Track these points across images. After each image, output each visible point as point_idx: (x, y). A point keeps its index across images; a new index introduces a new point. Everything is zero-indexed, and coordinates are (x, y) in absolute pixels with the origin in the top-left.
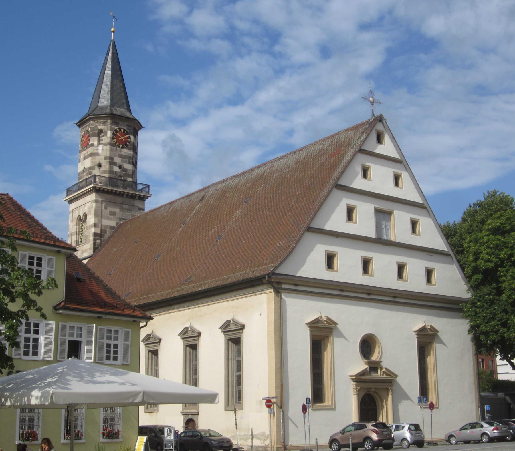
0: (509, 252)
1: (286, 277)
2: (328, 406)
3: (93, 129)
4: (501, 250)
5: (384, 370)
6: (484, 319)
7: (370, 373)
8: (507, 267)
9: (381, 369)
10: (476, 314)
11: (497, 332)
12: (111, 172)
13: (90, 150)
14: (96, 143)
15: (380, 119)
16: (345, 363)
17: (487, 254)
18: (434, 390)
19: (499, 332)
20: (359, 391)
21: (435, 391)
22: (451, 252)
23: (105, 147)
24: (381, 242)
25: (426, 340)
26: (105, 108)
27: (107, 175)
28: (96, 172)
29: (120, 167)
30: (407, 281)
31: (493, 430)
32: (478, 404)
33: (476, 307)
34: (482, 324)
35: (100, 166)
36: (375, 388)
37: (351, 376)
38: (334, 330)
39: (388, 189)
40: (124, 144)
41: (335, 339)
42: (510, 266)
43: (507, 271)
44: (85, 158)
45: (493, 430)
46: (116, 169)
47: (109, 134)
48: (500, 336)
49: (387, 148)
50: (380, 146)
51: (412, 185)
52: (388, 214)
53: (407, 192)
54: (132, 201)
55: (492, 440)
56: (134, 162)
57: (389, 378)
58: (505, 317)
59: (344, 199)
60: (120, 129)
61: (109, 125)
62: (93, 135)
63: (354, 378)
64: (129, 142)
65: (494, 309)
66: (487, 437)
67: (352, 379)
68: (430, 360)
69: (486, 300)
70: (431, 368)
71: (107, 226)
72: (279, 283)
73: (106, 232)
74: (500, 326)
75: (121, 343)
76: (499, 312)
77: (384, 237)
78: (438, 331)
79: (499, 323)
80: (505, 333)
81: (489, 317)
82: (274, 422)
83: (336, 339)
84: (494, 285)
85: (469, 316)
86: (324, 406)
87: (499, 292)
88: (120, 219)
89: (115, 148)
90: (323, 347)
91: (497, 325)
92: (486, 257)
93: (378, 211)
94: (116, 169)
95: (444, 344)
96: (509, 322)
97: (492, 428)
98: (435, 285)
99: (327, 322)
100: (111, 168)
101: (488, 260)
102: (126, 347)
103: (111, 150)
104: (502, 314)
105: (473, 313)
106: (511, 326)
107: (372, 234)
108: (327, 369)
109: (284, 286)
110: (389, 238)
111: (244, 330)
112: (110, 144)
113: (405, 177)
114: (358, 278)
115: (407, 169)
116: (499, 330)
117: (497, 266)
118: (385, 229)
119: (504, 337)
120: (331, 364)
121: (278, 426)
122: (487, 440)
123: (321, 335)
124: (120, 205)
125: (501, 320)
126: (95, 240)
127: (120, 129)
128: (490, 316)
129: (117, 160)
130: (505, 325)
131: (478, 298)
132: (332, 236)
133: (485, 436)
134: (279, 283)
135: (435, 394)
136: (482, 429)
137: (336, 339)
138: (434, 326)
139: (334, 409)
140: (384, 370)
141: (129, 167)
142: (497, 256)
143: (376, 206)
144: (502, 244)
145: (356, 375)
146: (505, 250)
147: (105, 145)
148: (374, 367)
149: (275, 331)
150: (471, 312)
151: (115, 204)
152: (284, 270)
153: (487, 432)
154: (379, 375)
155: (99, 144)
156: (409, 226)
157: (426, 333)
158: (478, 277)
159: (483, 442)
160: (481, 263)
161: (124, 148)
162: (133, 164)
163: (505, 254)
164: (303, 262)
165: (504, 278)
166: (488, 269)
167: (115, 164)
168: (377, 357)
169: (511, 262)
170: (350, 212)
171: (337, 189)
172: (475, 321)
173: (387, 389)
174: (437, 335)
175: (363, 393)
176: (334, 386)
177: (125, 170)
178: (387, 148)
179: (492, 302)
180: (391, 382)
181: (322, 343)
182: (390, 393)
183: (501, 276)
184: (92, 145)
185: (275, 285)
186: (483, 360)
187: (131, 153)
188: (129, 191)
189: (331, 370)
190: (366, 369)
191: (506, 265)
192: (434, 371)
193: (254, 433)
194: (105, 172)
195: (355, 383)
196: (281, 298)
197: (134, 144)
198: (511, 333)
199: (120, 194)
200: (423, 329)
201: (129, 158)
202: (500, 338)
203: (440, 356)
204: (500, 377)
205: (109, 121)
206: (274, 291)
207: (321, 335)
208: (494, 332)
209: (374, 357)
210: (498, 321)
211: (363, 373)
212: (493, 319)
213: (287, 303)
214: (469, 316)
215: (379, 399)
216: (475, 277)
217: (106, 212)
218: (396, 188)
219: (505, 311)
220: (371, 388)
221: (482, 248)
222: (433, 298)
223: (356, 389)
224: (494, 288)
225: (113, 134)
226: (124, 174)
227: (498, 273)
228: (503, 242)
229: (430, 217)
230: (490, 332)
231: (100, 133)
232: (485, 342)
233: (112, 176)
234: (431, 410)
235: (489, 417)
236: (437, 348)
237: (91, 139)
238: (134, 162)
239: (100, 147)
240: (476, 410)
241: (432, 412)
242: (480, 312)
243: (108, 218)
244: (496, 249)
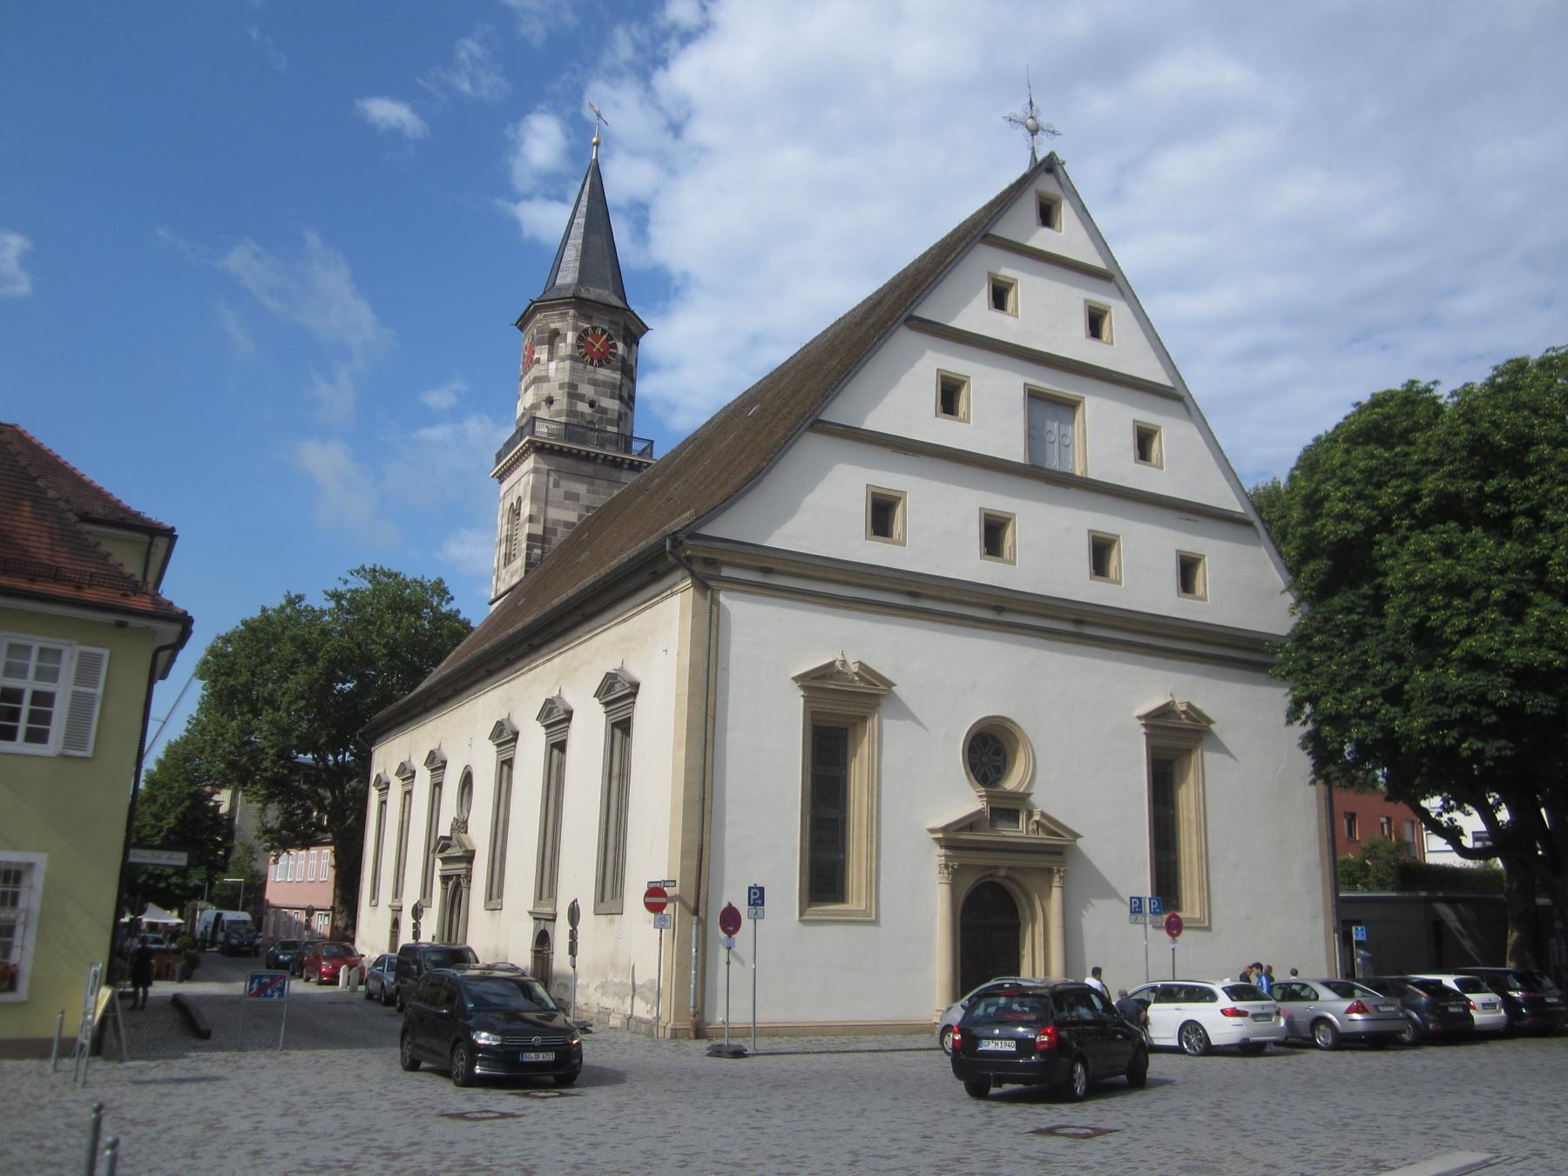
0: (1405, 488)
1: (730, 546)
2: (856, 912)
3: (540, 331)
4: (1379, 486)
5: (1036, 818)
6: (1332, 681)
7: (993, 824)
8: (1402, 532)
9: (1030, 815)
10: (1310, 666)
11: (1370, 717)
12: (572, 413)
13: (535, 371)
14: (544, 357)
15: (1049, 166)
16: (916, 793)
17: (1342, 499)
18: (1196, 880)
19: (1378, 717)
20: (955, 874)
21: (1201, 884)
22: (1253, 517)
23: (561, 365)
24: (1040, 474)
25: (1173, 745)
26: (569, 286)
27: (563, 419)
28: (543, 413)
29: (592, 404)
30: (1119, 583)
31: (1350, 1010)
32: (1331, 924)
33: (1310, 649)
34: (1324, 694)
35: (550, 401)
36: (1010, 868)
37: (932, 831)
38: (884, 703)
39: (1073, 343)
40: (603, 360)
41: (886, 722)
42: (1411, 528)
43: (1403, 541)
44: (526, 390)
45: (1350, 1010)
46: (583, 407)
47: (571, 337)
48: (1382, 729)
49: (1066, 239)
50: (1046, 231)
51: (1140, 338)
52: (1070, 406)
53: (1123, 350)
54: (614, 473)
55: (1345, 1042)
56: (625, 394)
57: (1053, 840)
58: (1394, 673)
59: (929, 353)
60: (594, 328)
61: (570, 320)
62: (540, 342)
63: (940, 835)
64: (614, 355)
65: (1365, 653)
66: (1329, 1031)
67: (937, 840)
68: (1186, 796)
69: (1337, 626)
70: (1189, 820)
71: (557, 522)
72: (711, 563)
73: (555, 532)
74: (1380, 700)
75: (64, 690)
76: (1378, 659)
77: (1053, 463)
78: (1210, 721)
79: (1377, 691)
80: (1395, 718)
81: (1346, 675)
82: (669, 950)
83: (887, 723)
84: (1366, 589)
85: (1289, 673)
86: (848, 913)
87: (1378, 601)
88: (588, 508)
89: (581, 366)
90: (850, 752)
91: (1372, 697)
92: (1340, 507)
93: (1035, 397)
94: (583, 407)
95: (1228, 753)
96: (1407, 687)
97: (1347, 1004)
98: (1204, 599)
99: (862, 679)
100: (570, 404)
101: (1346, 516)
102: (80, 705)
103: (573, 370)
104: (1388, 666)
105: (1302, 664)
106: (1412, 699)
107: (1014, 450)
108: (860, 809)
109: (726, 572)
110: (1068, 469)
111: (639, 697)
112: (572, 358)
113: (1119, 316)
114: (964, 562)
115: (1126, 292)
116: (1377, 711)
117: (1371, 530)
118: (1056, 445)
119: (1392, 731)
120: (870, 795)
121: (682, 966)
122: (1330, 1041)
123: (838, 720)
124: (590, 479)
125: (1382, 682)
126: (529, 548)
127: (594, 328)
128: (1348, 671)
129: (586, 390)
130: (1395, 696)
131: (1315, 624)
132: (888, 451)
133: (1322, 1027)
134: (711, 563)
135: (1201, 890)
136: (1312, 1005)
137: (887, 723)
138: (1198, 706)
139: (875, 922)
140: (1036, 818)
141: (612, 405)
142: (1370, 500)
143: (1032, 381)
144: (1386, 469)
145: (944, 829)
146: (1394, 483)
147: (563, 359)
148: (1007, 809)
149: (691, 695)
150: (1295, 661)
151: (579, 476)
152: (732, 526)
153: (1330, 1016)
154: (1021, 831)
155: (550, 359)
156: (1129, 441)
157: (1171, 723)
158: (1321, 564)
159: (1317, 1047)
160: (1323, 526)
161: (601, 365)
162: (621, 398)
163: (1393, 494)
164: (790, 511)
165: (1390, 562)
166: (1344, 540)
167: (581, 398)
168: (1021, 783)
169: (1412, 515)
170: (950, 395)
171: (910, 327)
172: (1306, 685)
173: (1050, 872)
174: (1208, 732)
175: (969, 882)
176: (875, 856)
177: (604, 411)
178: (1066, 239)
179: (1358, 633)
180: (1061, 854)
181: (850, 738)
182: (1056, 881)
183: (1384, 558)
184: (538, 361)
185: (697, 568)
186: (1389, 820)
187: (617, 376)
188: (610, 452)
189: (870, 810)
190: (980, 812)
191: (1399, 526)
192: (1199, 827)
193: (638, 982)
194: (559, 413)
195: (943, 851)
196: (715, 602)
197: (624, 360)
198: (1414, 717)
199: (589, 458)
200: (1165, 711)
201: (613, 386)
202: (1379, 735)
203: (1210, 786)
204: (1431, 859)
205: (572, 312)
206: (694, 585)
207: (838, 720)
208: (1362, 717)
209: (1012, 783)
210: (1375, 684)
211: (969, 824)
212: (1358, 679)
213: (733, 618)
214: (1289, 673)
215: (1024, 900)
216: (1311, 566)
217: (557, 494)
218: (1094, 342)
219: (1399, 659)
220: (996, 867)
221: (1328, 487)
222: (1200, 631)
223: (947, 866)
224: (1365, 597)
225: (580, 338)
226: (601, 419)
227: (1375, 552)
228: (1387, 461)
229: (1193, 421)
230: (1350, 717)
231: (553, 337)
232: (1336, 745)
233: (574, 421)
234: (1174, 936)
235: (1364, 959)
236: (1207, 761)
237: (537, 349)
238: (625, 394)
239: (553, 365)
240: (1327, 938)
241: (1174, 941)
242: (1321, 663)
243: (560, 506)
244: (1368, 483)
